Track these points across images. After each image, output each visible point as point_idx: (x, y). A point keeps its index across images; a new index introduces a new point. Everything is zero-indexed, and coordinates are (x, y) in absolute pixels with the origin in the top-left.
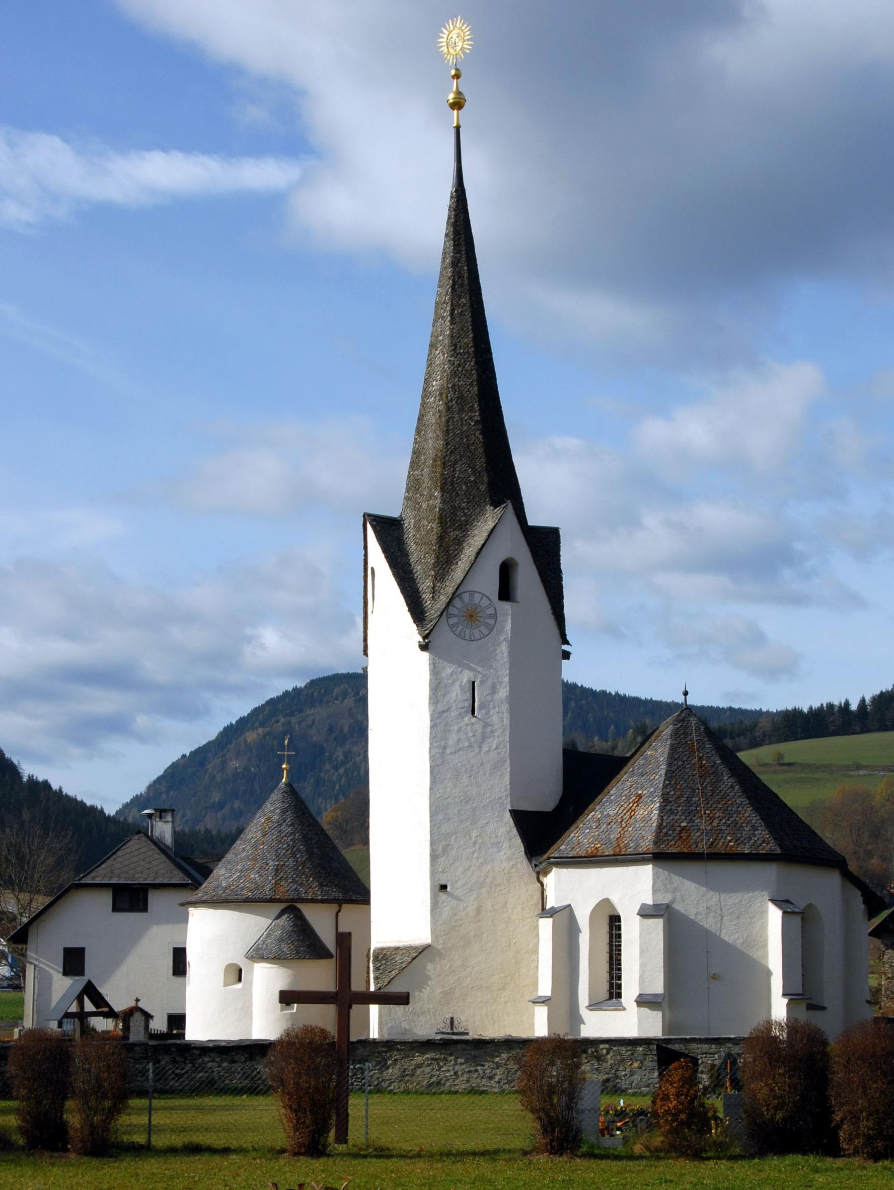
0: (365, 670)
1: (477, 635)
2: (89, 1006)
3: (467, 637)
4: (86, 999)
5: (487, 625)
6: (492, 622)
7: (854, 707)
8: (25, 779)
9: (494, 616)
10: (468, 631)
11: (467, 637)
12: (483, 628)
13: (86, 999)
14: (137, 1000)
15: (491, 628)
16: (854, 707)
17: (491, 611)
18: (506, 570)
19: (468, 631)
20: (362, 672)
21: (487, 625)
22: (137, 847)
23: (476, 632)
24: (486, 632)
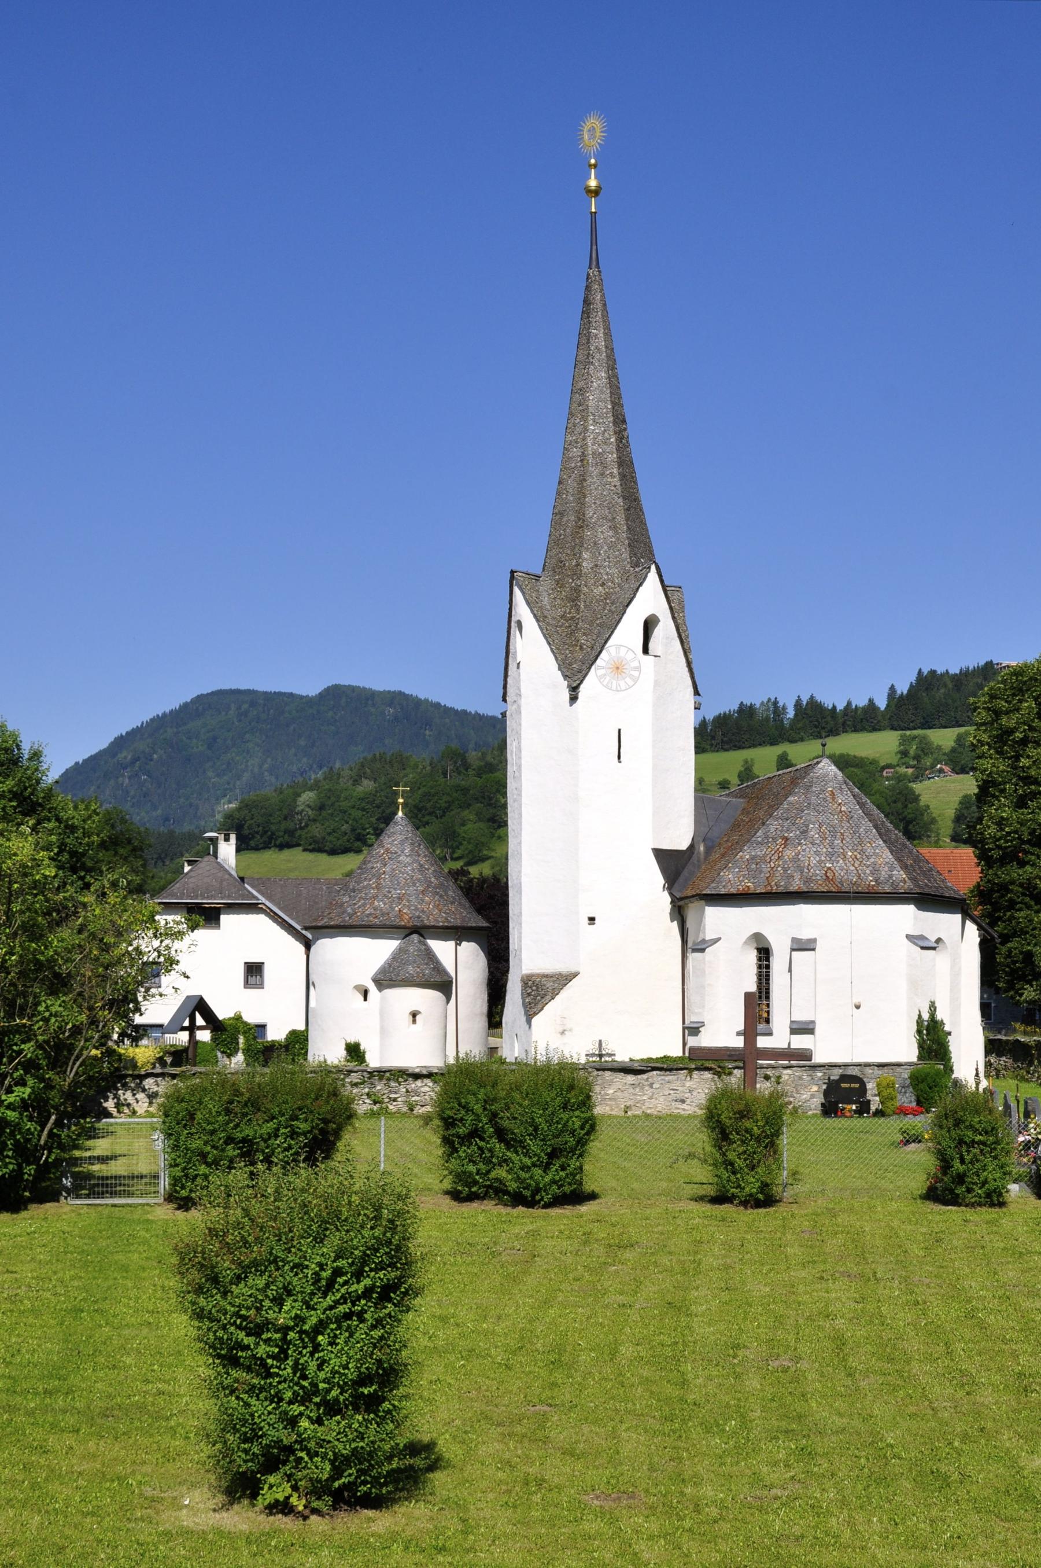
0: (504, 715)
1: (623, 686)
2: (200, 1021)
3: (614, 688)
4: (198, 1015)
5: (631, 677)
6: (636, 674)
7: (882, 703)
8: (233, 837)
9: (638, 669)
10: (614, 682)
11: (614, 688)
12: (628, 680)
13: (198, 1015)
14: (571, 1030)
15: (636, 680)
16: (882, 703)
17: (635, 664)
18: (649, 626)
19: (608, 678)
20: (500, 716)
21: (631, 677)
22: (208, 868)
23: (622, 683)
24: (631, 683)
